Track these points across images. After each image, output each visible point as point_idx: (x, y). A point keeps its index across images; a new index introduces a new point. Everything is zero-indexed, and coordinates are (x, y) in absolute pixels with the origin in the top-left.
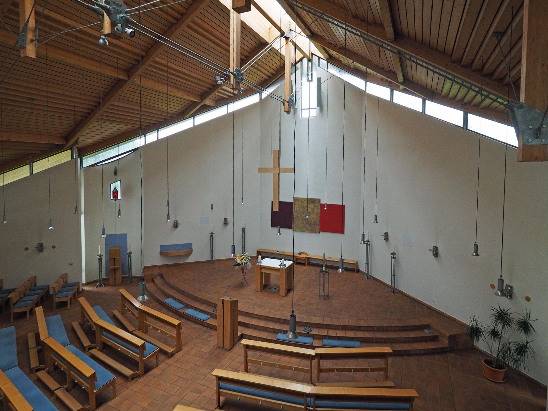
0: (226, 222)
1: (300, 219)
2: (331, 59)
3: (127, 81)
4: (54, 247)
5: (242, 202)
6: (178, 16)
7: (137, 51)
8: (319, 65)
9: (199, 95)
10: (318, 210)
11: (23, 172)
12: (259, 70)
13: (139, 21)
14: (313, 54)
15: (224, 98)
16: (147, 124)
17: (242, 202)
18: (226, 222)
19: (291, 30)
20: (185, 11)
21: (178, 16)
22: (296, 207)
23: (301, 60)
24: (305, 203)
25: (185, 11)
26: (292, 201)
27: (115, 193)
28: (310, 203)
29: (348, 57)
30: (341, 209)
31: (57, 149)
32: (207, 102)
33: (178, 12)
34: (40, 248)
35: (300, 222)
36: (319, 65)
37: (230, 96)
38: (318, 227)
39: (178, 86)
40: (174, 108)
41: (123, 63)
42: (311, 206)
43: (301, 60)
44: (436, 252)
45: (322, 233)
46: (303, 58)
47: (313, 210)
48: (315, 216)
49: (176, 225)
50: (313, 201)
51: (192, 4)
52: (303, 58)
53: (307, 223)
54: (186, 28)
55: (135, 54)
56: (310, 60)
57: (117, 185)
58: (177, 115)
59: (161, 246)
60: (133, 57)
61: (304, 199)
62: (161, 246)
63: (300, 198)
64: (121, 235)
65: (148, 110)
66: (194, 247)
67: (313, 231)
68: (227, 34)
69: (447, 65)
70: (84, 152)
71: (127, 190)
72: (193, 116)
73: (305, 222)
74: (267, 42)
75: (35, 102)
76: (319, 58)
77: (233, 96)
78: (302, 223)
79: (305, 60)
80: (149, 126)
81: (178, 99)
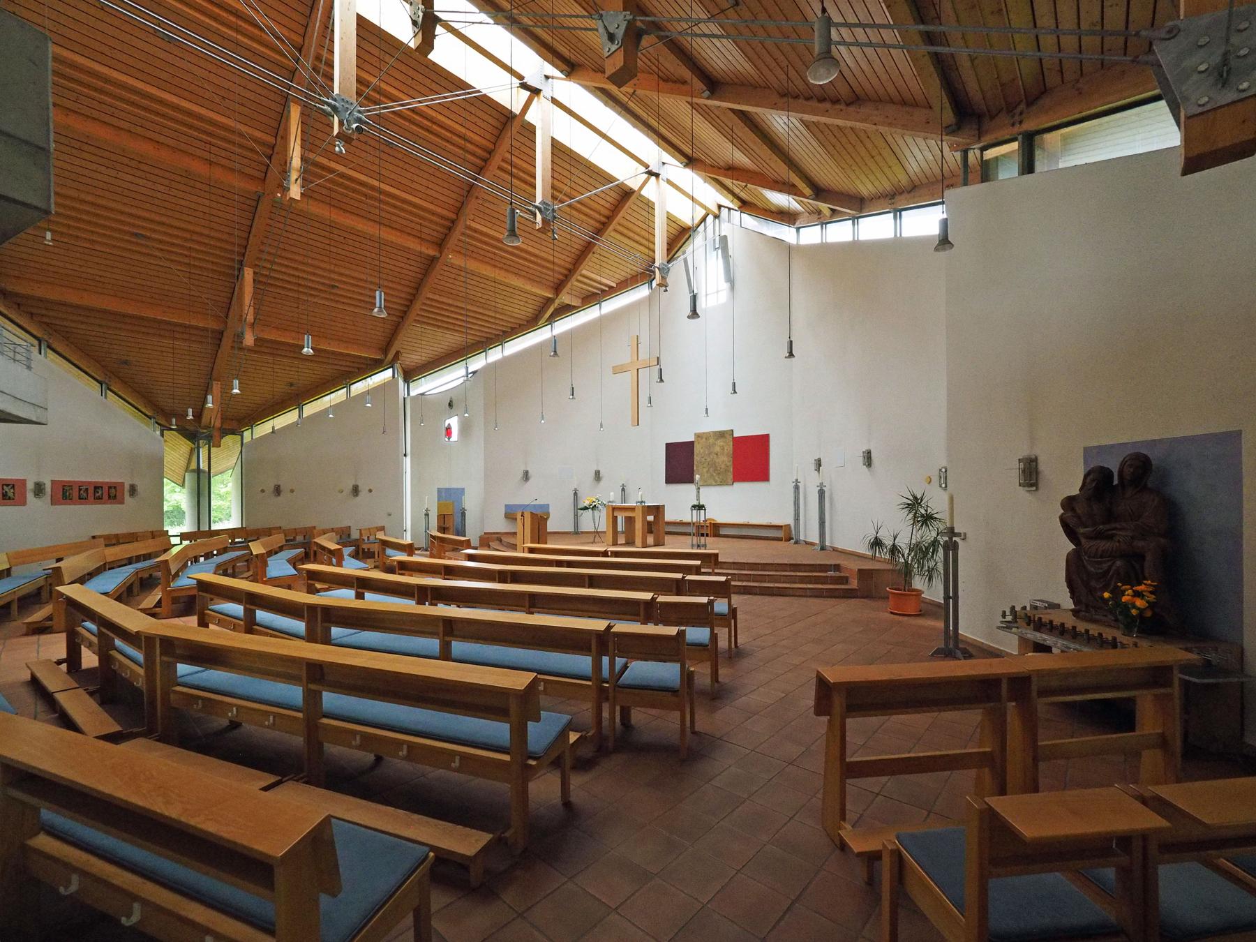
0: (598, 475)
1: (705, 465)
2: (745, 206)
3: (439, 258)
4: (370, 491)
5: (602, 426)
6: (485, 155)
7: (445, 213)
8: (729, 221)
9: (552, 287)
10: (729, 448)
11: (339, 396)
12: (626, 236)
13: (378, 122)
14: (720, 207)
15: (594, 294)
16: (488, 336)
17: (602, 426)
18: (598, 475)
19: (664, 163)
20: (491, 146)
21: (485, 155)
22: (698, 449)
23: (704, 219)
24: (711, 440)
25: (491, 146)
26: (691, 439)
27: (448, 431)
28: (717, 439)
29: (737, 180)
30: (761, 443)
31: (375, 366)
32: (565, 298)
33: (484, 150)
34: (356, 491)
35: (705, 470)
36: (729, 221)
37: (603, 291)
38: (731, 476)
39: (516, 271)
40: (524, 310)
41: (430, 232)
42: (720, 442)
43: (704, 219)
44: (868, 458)
45: (739, 486)
46: (707, 215)
47: (723, 449)
48: (725, 459)
49: (526, 476)
50: (721, 434)
51: (500, 135)
52: (707, 215)
53: (714, 471)
54: (498, 171)
55: (442, 217)
56: (717, 217)
57: (454, 422)
58: (528, 321)
59: (506, 506)
60: (442, 222)
61: (709, 433)
62: (506, 506)
63: (704, 433)
64: (457, 489)
65: (481, 311)
66: (551, 510)
67: (723, 483)
68: (531, 153)
69: (775, 104)
70: (410, 375)
71: (465, 428)
72: (550, 321)
73: (711, 469)
74: (631, 189)
75: (334, 291)
76: (730, 209)
77: (607, 289)
78: (707, 472)
79: (710, 219)
80: (491, 339)
81: (522, 294)
